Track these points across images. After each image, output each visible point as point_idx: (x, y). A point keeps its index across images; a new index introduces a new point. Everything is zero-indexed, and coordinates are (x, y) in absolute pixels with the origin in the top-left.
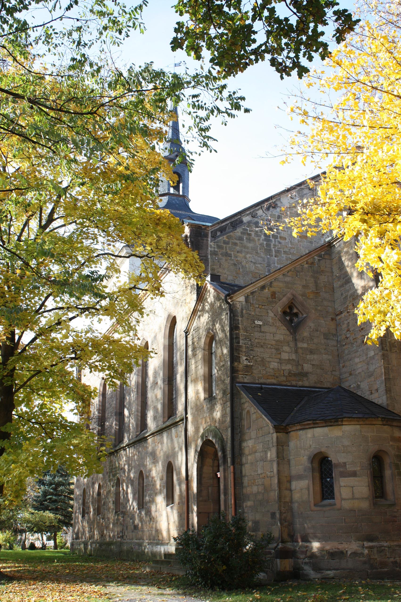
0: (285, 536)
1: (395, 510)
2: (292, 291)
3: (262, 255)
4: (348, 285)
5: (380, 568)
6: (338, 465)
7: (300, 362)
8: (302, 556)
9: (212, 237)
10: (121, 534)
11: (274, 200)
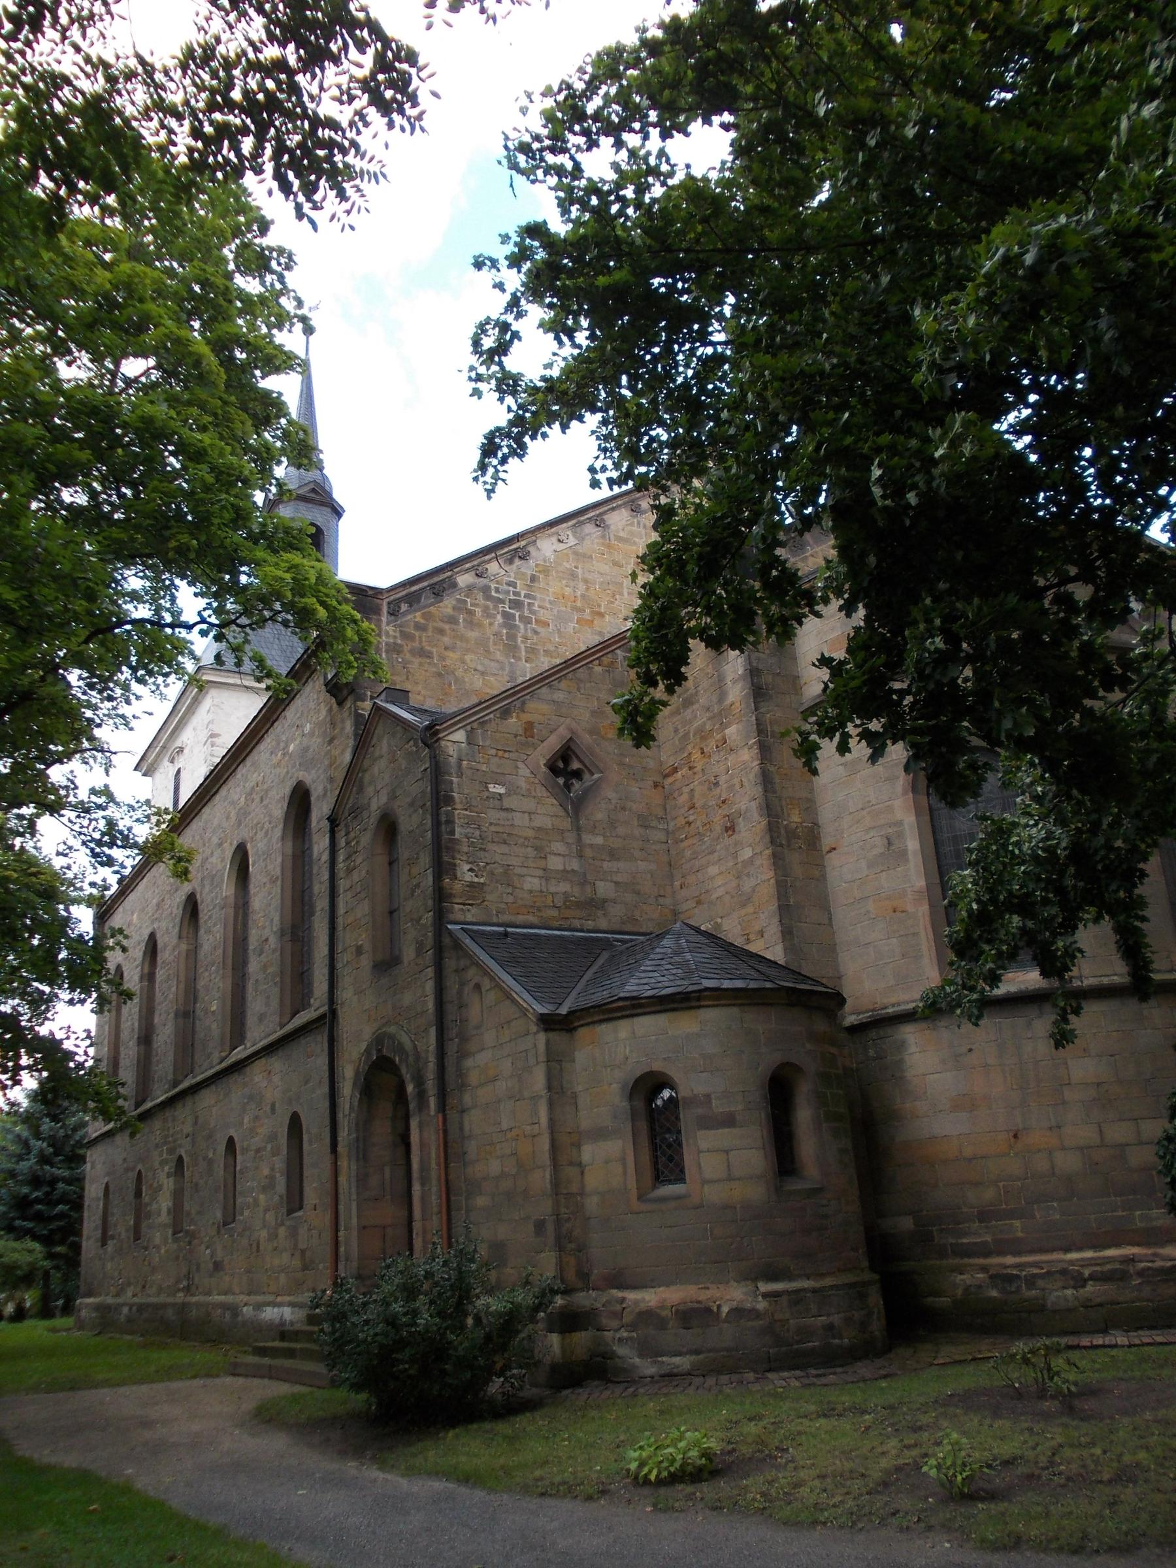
0: (571, 1275)
1: (824, 1202)
2: (568, 721)
3: (499, 656)
4: (689, 711)
5: (798, 1342)
6: (692, 1101)
7: (589, 877)
8: (615, 1324)
9: (390, 614)
10: (185, 1283)
11: (523, 543)
